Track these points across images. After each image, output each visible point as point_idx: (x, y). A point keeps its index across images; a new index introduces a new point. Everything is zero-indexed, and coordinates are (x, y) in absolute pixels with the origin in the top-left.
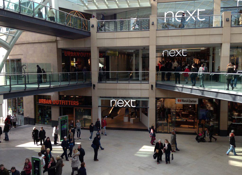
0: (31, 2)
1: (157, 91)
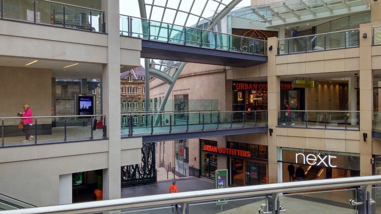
0: (195, 30)
1: (375, 144)
